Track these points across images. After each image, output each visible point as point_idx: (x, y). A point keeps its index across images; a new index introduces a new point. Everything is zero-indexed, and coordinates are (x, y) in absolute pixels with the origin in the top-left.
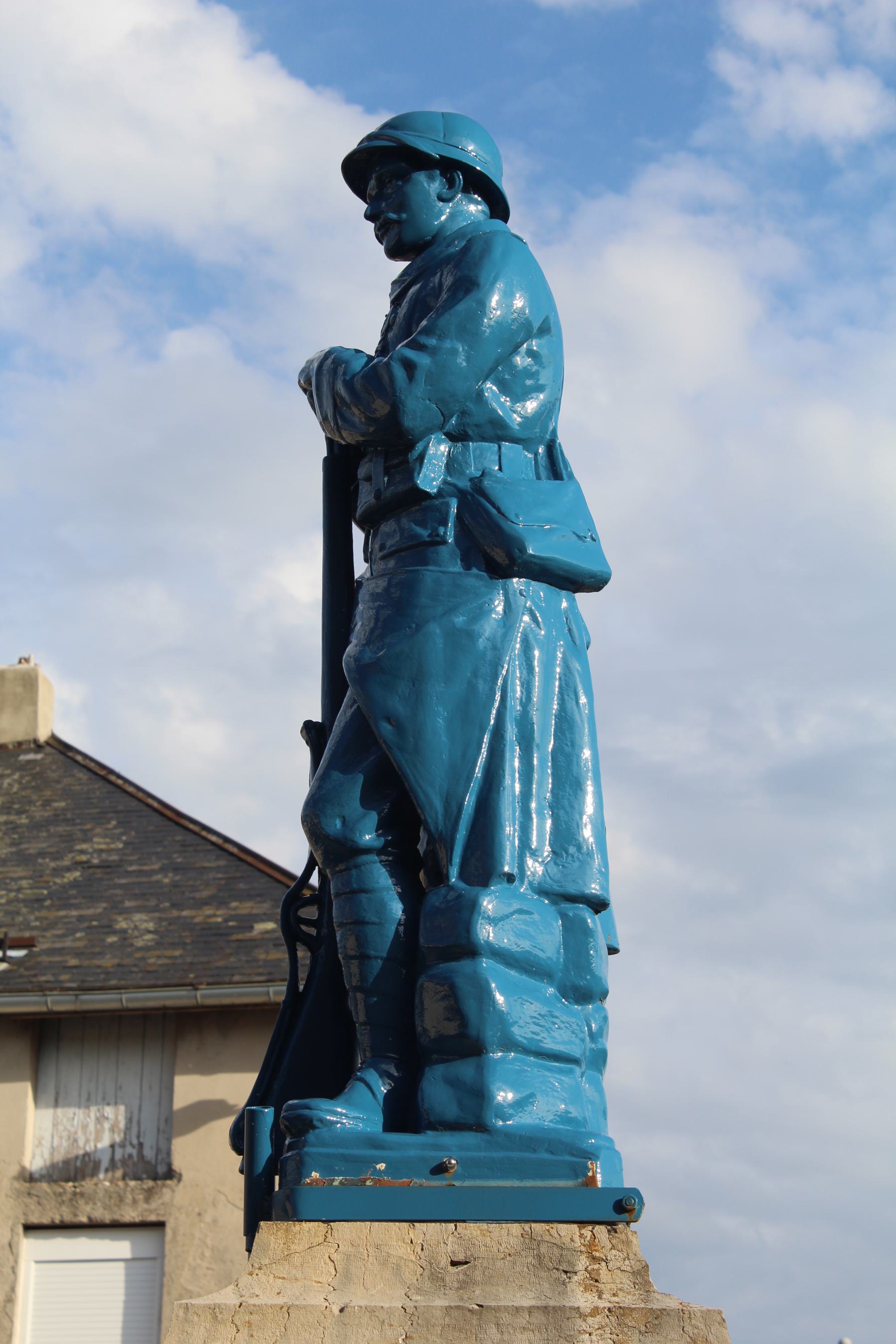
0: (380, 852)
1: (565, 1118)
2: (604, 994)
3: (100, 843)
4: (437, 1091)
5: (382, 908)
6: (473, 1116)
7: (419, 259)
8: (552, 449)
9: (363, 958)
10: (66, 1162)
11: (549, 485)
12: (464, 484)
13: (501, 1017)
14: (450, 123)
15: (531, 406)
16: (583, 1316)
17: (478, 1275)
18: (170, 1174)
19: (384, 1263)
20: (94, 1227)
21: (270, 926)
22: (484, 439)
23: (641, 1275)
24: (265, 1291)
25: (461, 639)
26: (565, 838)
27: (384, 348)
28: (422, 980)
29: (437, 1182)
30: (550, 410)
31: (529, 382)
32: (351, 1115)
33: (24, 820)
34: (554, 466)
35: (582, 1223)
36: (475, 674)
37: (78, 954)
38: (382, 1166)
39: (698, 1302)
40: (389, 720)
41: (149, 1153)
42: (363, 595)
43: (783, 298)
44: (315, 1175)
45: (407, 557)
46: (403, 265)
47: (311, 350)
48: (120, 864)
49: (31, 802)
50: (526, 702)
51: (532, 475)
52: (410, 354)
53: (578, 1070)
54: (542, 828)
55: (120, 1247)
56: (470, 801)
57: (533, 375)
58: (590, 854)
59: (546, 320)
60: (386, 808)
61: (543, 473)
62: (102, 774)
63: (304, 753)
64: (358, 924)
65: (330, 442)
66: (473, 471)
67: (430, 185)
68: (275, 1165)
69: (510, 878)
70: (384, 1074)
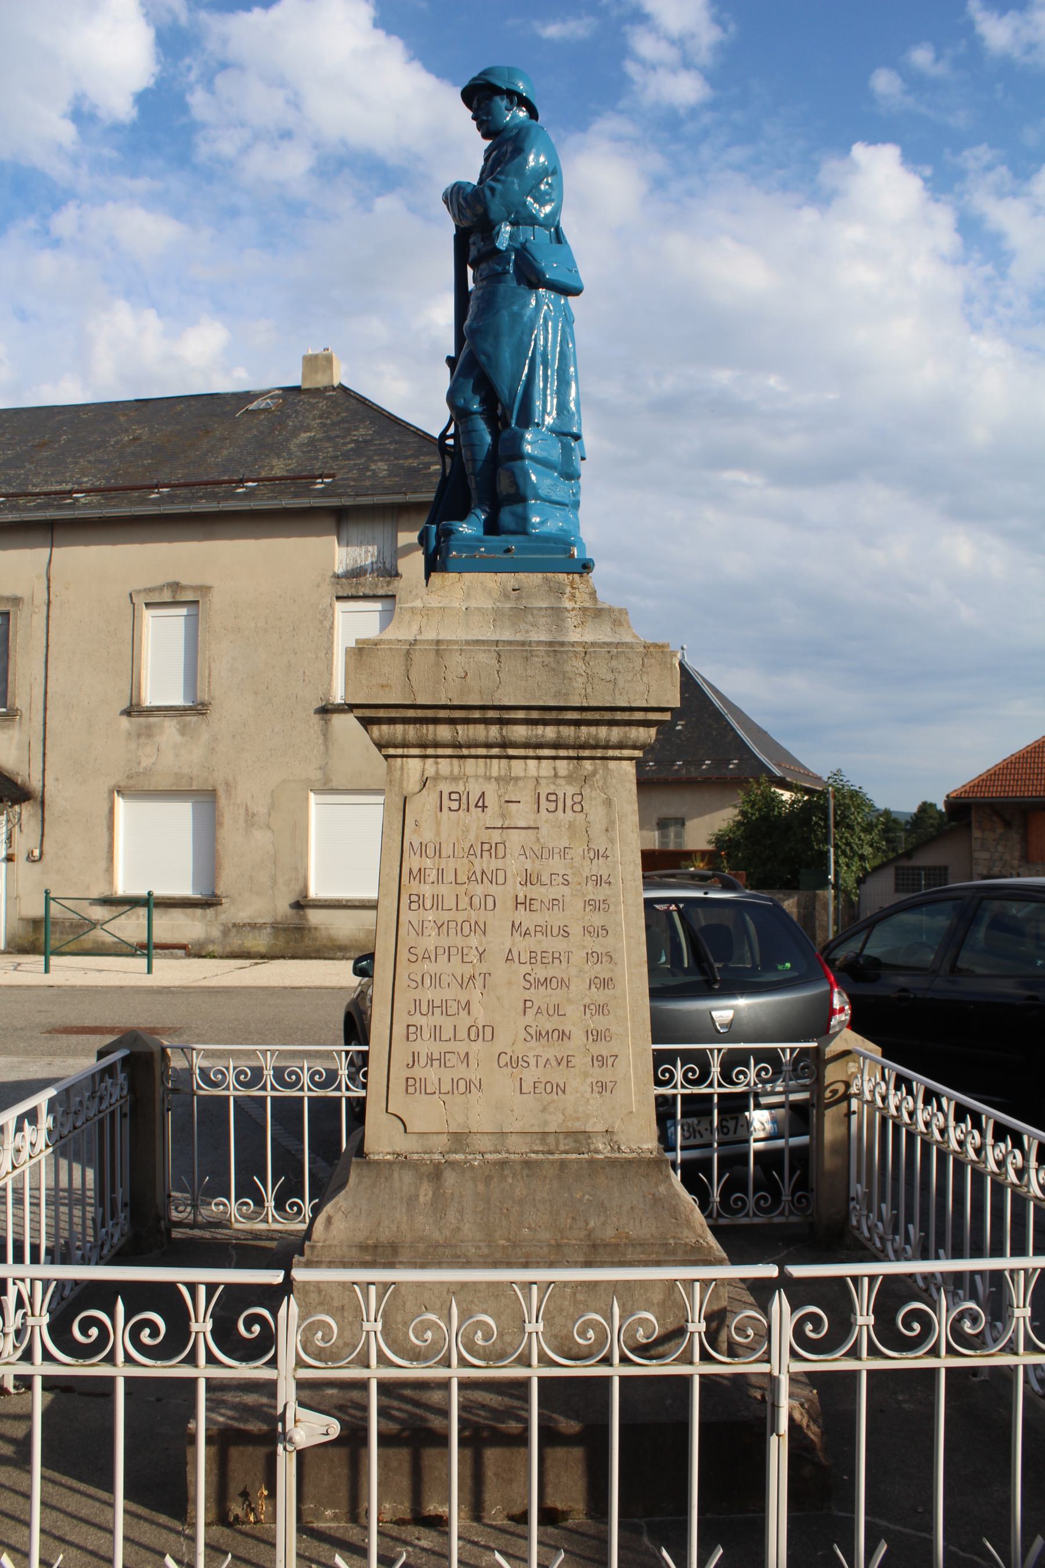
0: (481, 413)
1: (561, 529)
2: (579, 477)
3: (362, 431)
4: (506, 517)
5: (482, 438)
6: (522, 528)
7: (497, 140)
8: (558, 230)
9: (474, 460)
10: (353, 570)
11: (555, 246)
12: (518, 246)
13: (534, 485)
14: (511, 72)
15: (548, 209)
16: (568, 611)
17: (524, 594)
18: (397, 575)
19: (484, 590)
20: (365, 597)
21: (438, 467)
22: (526, 225)
23: (593, 594)
24: (434, 601)
25: (516, 317)
26: (562, 407)
27: (481, 181)
28: (500, 469)
29: (506, 556)
30: (556, 212)
31: (547, 198)
32: (467, 529)
33: (329, 422)
34: (559, 237)
35: (568, 573)
36: (523, 333)
37: (354, 480)
38: (483, 549)
39: (616, 605)
40: (484, 354)
41: (388, 566)
42: (472, 297)
43: (658, 184)
44: (454, 553)
45: (491, 280)
46: (489, 142)
47: (448, 181)
48: (371, 441)
49: (331, 414)
50: (545, 346)
51: (548, 242)
52: (493, 184)
53: (567, 509)
54: (552, 403)
55: (378, 606)
56: (520, 389)
57: (549, 194)
58: (573, 414)
59: (555, 168)
60: (483, 393)
61: (553, 240)
62: (363, 401)
63: (447, 370)
64: (471, 446)
65: (457, 227)
66: (521, 239)
67: (502, 103)
68: (437, 550)
69: (538, 425)
70: (484, 511)
